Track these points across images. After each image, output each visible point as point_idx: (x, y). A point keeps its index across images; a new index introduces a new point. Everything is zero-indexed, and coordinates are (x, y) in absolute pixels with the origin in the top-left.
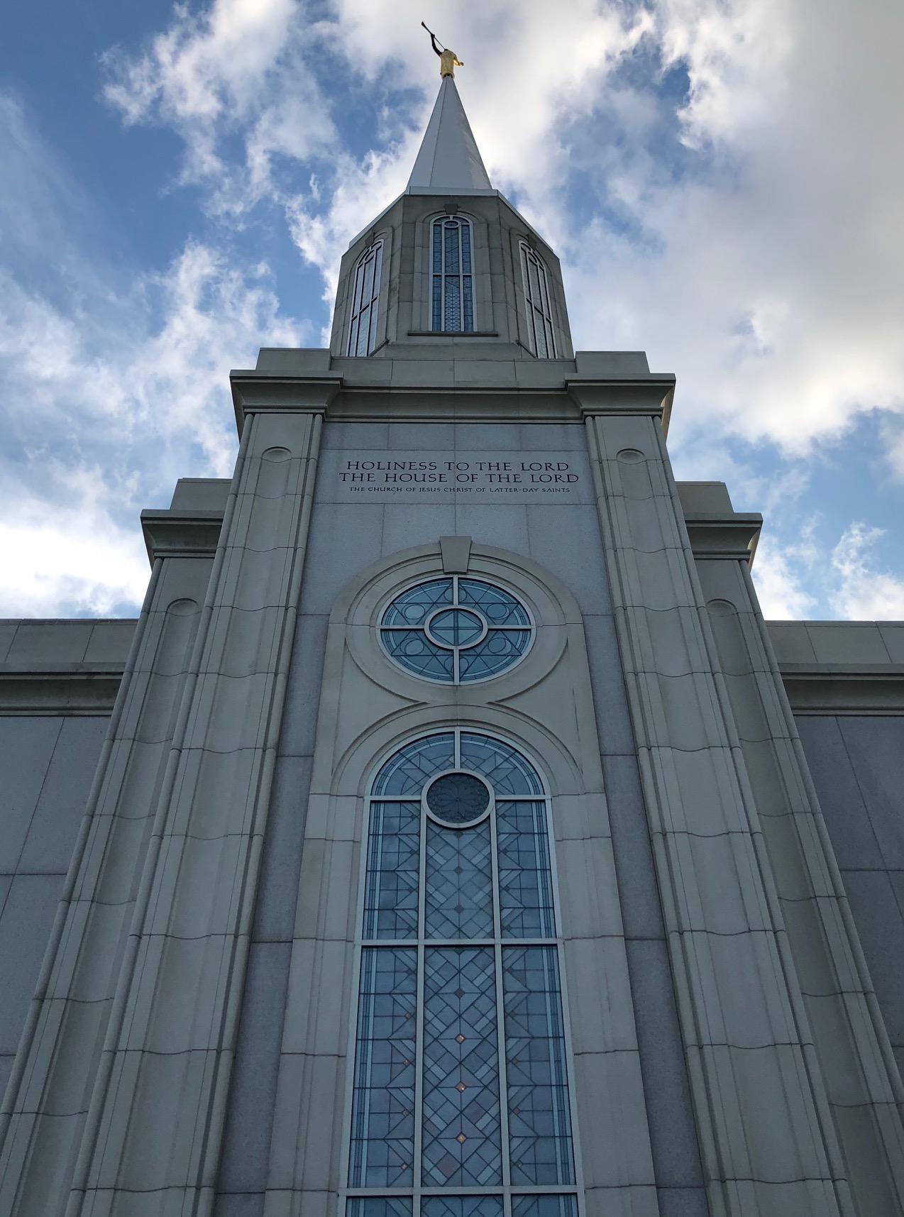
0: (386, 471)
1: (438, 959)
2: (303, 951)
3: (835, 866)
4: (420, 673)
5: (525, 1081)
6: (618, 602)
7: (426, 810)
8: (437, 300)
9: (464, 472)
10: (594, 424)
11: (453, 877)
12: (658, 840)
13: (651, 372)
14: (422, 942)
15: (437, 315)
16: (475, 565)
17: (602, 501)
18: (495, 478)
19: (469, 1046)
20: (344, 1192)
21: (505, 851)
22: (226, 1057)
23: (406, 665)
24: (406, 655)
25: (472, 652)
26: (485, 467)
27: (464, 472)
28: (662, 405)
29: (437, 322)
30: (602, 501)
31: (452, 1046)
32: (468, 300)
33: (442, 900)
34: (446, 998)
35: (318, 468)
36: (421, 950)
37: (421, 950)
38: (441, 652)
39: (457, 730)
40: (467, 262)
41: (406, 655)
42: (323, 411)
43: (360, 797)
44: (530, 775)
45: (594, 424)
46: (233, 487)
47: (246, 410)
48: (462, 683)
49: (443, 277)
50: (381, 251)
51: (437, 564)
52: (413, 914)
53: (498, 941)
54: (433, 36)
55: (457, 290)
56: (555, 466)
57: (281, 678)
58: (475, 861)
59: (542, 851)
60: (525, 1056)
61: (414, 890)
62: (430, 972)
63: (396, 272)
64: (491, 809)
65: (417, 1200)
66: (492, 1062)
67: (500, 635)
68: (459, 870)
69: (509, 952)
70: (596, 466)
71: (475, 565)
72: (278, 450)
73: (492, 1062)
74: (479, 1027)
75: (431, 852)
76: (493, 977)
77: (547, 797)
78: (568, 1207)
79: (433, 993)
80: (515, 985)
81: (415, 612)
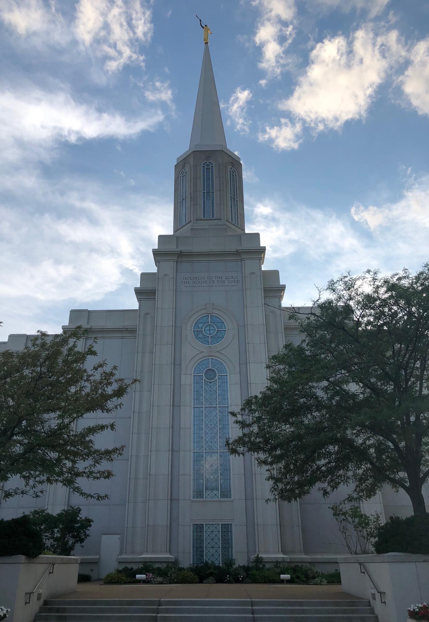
0: (193, 280)
1: (207, 409)
2: (182, 453)
3: (283, 321)
4: (202, 343)
5: (221, 390)
6: (246, 323)
7: (204, 378)
8: (204, 204)
9: (211, 280)
10: (244, 262)
11: (209, 392)
12: (249, 385)
13: (261, 246)
14: (204, 406)
15: (204, 214)
16: (214, 311)
17: (244, 290)
18: (219, 282)
19: (213, 426)
20: (193, 375)
21: (220, 387)
22: (171, 429)
23: (199, 340)
24: (199, 338)
25: (213, 337)
26: (217, 278)
27: (211, 280)
28: (262, 256)
29: (204, 217)
30: (244, 290)
31: (210, 426)
32: (213, 203)
33: (207, 397)
34: (209, 443)
35: (176, 280)
36: (204, 407)
37: (204, 407)
38: (206, 337)
39: (210, 358)
40: (213, 187)
41: (199, 338)
42: (176, 261)
43: (190, 451)
44: (225, 369)
45: (244, 262)
46: (157, 275)
47: (157, 261)
48: (212, 345)
49: (206, 193)
50: (187, 173)
51: (205, 311)
52: (202, 400)
53: (218, 406)
54: (200, 20)
55: (209, 198)
56: (234, 278)
57: (173, 346)
58: (214, 389)
59: (227, 386)
60: (222, 428)
61: (203, 456)
62: (206, 412)
63: (192, 190)
64: (217, 378)
65: (204, 453)
66: (216, 429)
67: (219, 331)
68: (211, 391)
69: (220, 408)
70: (244, 278)
71: (214, 311)
72: (166, 275)
73: (216, 429)
74: (214, 422)
75: (205, 387)
76: (218, 476)
77: (228, 374)
78: (227, 409)
79: (206, 416)
80: (221, 414)
81: (200, 325)
